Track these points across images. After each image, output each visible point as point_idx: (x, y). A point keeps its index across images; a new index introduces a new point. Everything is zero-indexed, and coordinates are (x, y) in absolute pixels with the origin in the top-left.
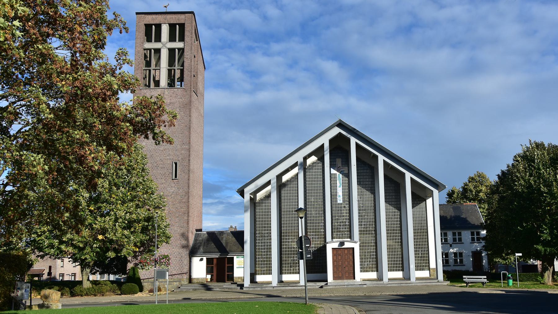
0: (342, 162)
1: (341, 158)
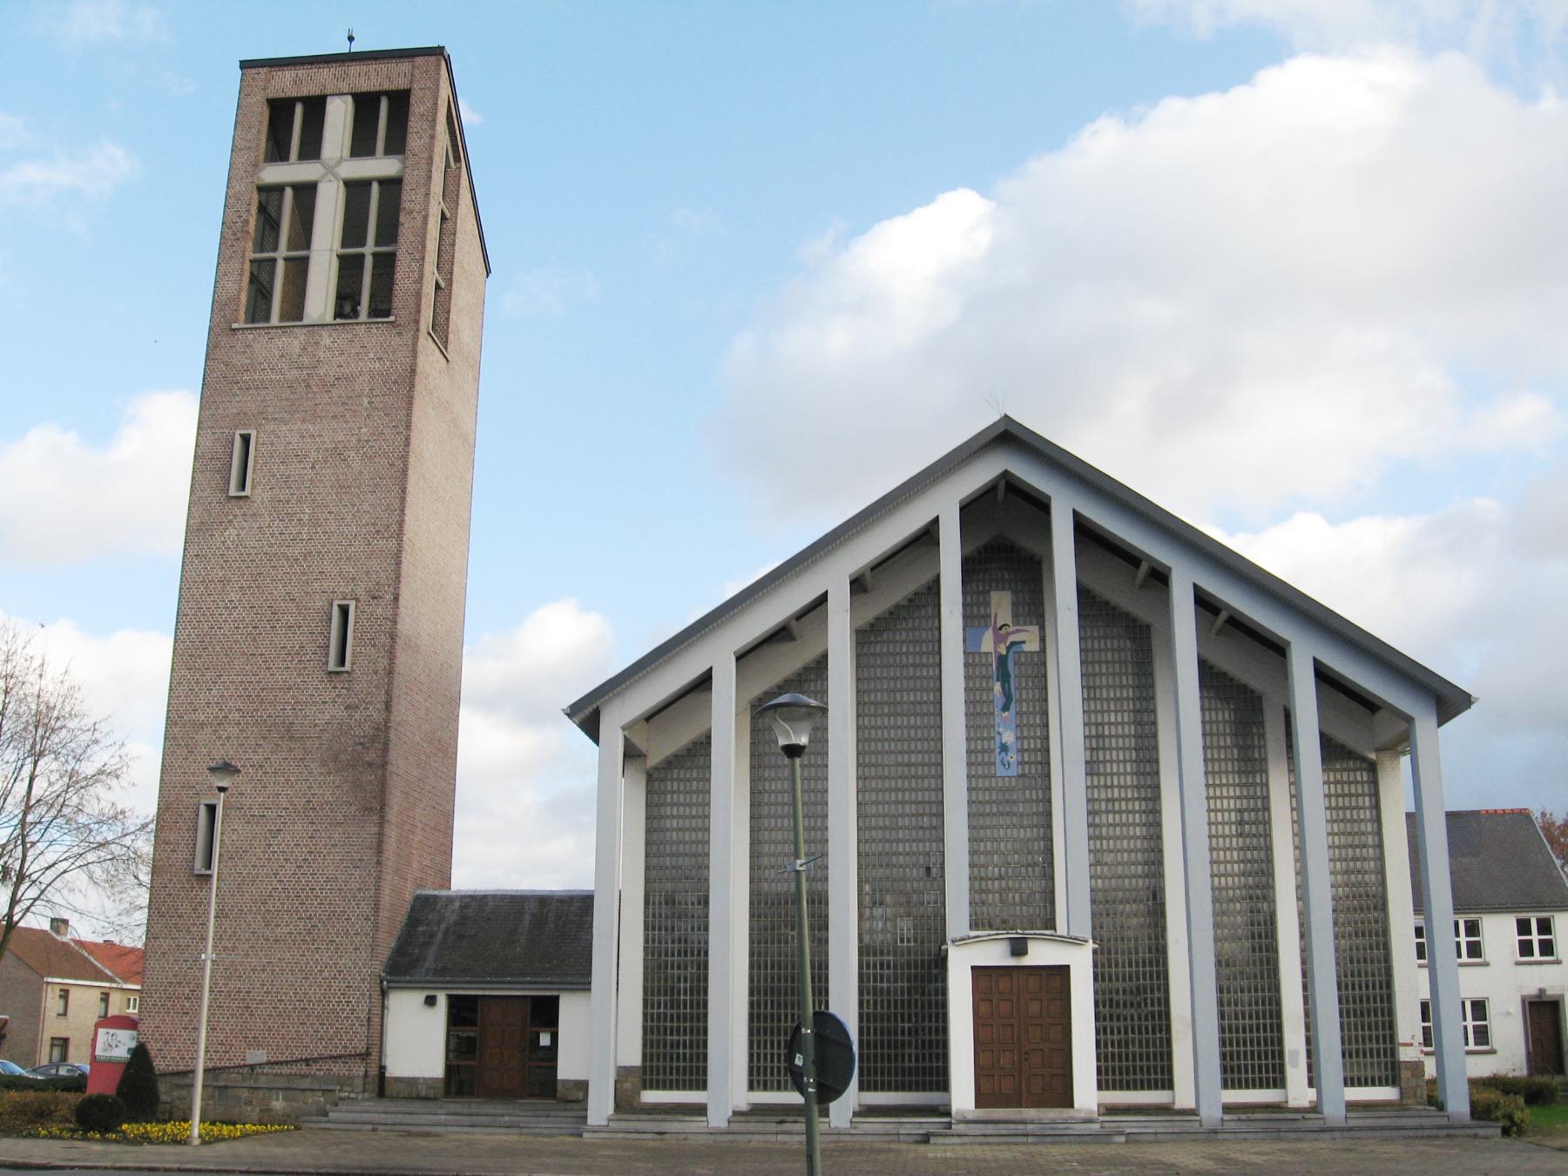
0: (1015, 604)
1: (1010, 589)
